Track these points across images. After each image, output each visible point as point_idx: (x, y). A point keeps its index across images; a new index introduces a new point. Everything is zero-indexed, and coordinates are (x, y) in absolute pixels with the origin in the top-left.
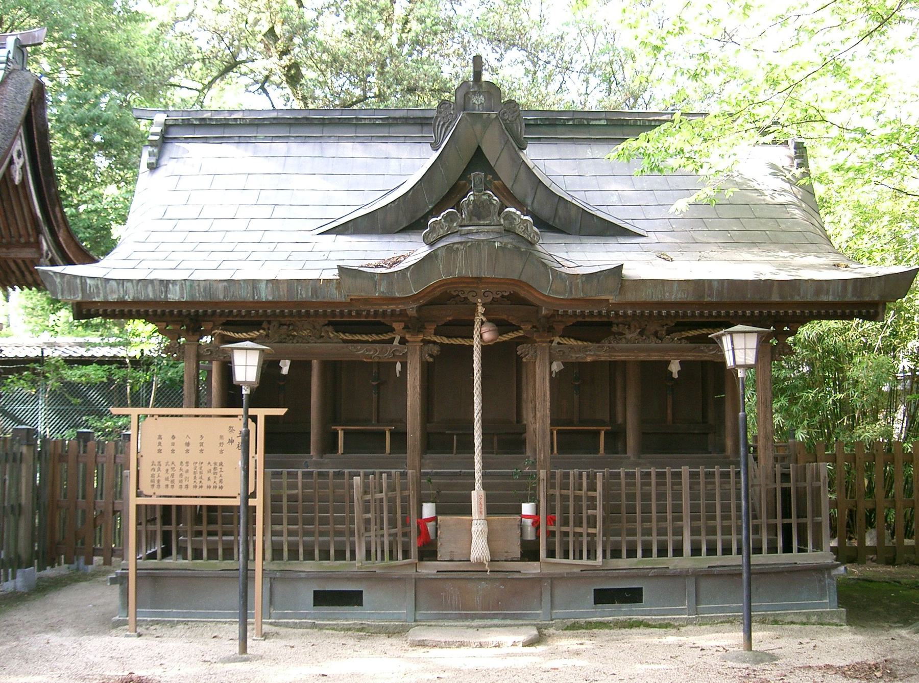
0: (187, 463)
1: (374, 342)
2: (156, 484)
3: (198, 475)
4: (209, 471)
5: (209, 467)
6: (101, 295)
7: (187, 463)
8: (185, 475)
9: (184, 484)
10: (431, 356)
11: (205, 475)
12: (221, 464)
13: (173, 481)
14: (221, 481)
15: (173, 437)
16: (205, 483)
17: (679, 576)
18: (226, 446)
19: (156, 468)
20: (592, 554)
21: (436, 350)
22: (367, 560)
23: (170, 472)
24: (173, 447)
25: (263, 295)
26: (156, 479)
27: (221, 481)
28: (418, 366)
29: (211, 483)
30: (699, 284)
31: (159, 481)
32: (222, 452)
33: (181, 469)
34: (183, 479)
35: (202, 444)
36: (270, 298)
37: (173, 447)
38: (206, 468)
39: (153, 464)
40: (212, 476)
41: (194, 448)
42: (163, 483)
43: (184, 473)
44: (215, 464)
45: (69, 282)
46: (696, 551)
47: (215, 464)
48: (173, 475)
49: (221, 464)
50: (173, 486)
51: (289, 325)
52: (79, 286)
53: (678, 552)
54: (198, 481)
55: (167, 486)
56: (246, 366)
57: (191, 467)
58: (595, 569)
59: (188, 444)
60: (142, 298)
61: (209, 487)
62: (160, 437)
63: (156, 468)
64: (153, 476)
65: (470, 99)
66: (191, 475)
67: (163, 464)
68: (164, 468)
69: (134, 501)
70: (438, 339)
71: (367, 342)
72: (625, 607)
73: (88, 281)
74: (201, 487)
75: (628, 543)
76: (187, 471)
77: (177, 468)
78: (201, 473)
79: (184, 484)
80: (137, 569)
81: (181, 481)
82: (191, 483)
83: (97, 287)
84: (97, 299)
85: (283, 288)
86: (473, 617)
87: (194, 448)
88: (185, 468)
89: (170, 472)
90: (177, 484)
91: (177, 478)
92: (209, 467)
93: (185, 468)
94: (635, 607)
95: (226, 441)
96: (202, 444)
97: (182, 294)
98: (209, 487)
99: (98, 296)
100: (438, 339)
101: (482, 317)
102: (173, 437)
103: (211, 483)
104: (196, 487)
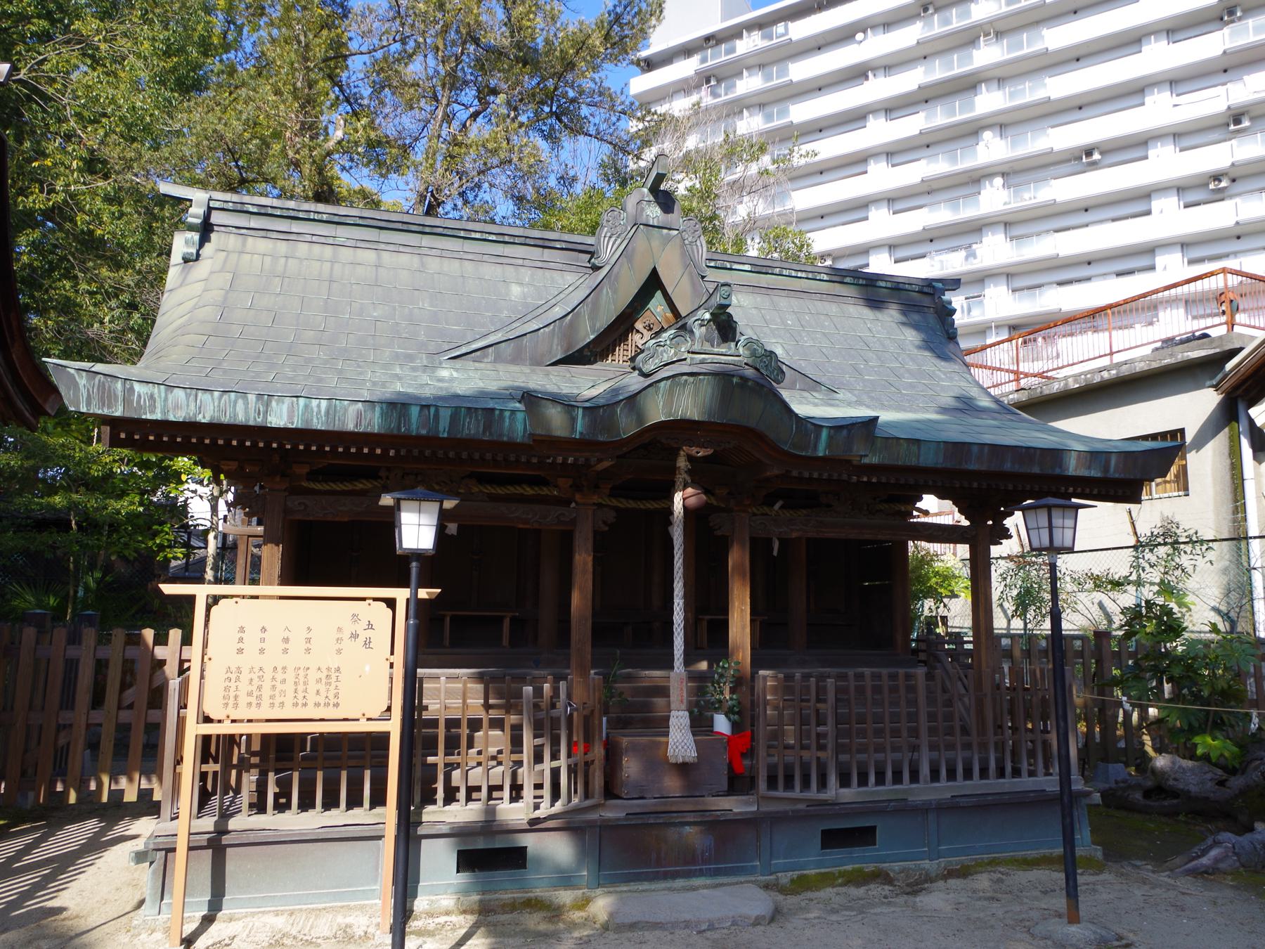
0: (284, 668)
1: (343, 493)
2: (231, 702)
3: (301, 688)
4: (319, 681)
5: (319, 675)
6: (158, 410)
7: (284, 668)
8: (279, 686)
9: (278, 700)
10: (605, 523)
11: (312, 687)
12: (338, 670)
13: (259, 697)
14: (336, 696)
15: (264, 630)
16: (312, 698)
17: (923, 810)
18: (347, 644)
19: (233, 677)
20: (823, 784)
21: (611, 516)
22: (133, 661)
23: (256, 682)
24: (263, 645)
25: (414, 426)
26: (232, 694)
27: (336, 696)
28: (591, 535)
29: (321, 700)
30: (997, 450)
31: (236, 697)
32: (339, 651)
33: (274, 679)
34: (277, 693)
35: (309, 640)
36: (424, 432)
37: (263, 645)
38: (313, 676)
39: (229, 670)
40: (322, 688)
41: (297, 645)
42: (243, 700)
43: (278, 685)
44: (329, 669)
45: (101, 386)
46: (935, 775)
47: (329, 669)
48: (259, 688)
49: (338, 670)
50: (259, 705)
51: (417, 475)
52: (120, 394)
53: (915, 777)
54: (300, 695)
55: (250, 704)
56: (417, 530)
57: (290, 676)
58: (824, 803)
59: (286, 640)
60: (225, 419)
61: (317, 705)
62: (242, 630)
63: (233, 677)
64: (227, 689)
65: (643, 209)
66: (289, 687)
67: (245, 671)
68: (245, 677)
69: (194, 730)
70: (615, 502)
71: (333, 493)
72: (858, 852)
73: (137, 387)
74: (305, 705)
75: (859, 764)
76: (284, 681)
77: (268, 674)
78: (305, 683)
79: (278, 700)
80: (190, 834)
81: (272, 697)
82: (289, 700)
83: (152, 397)
84: (149, 417)
85: (445, 415)
86: (674, 876)
87: (297, 645)
88: (279, 676)
89: (256, 682)
90: (266, 702)
91: (266, 692)
92: (319, 675)
93: (279, 676)
94: (869, 852)
95: (347, 635)
96: (309, 640)
97: (291, 416)
98: (317, 705)
99: (152, 412)
100: (615, 502)
101: (685, 476)
102: (264, 630)
103: (321, 700)
104: (296, 705)
